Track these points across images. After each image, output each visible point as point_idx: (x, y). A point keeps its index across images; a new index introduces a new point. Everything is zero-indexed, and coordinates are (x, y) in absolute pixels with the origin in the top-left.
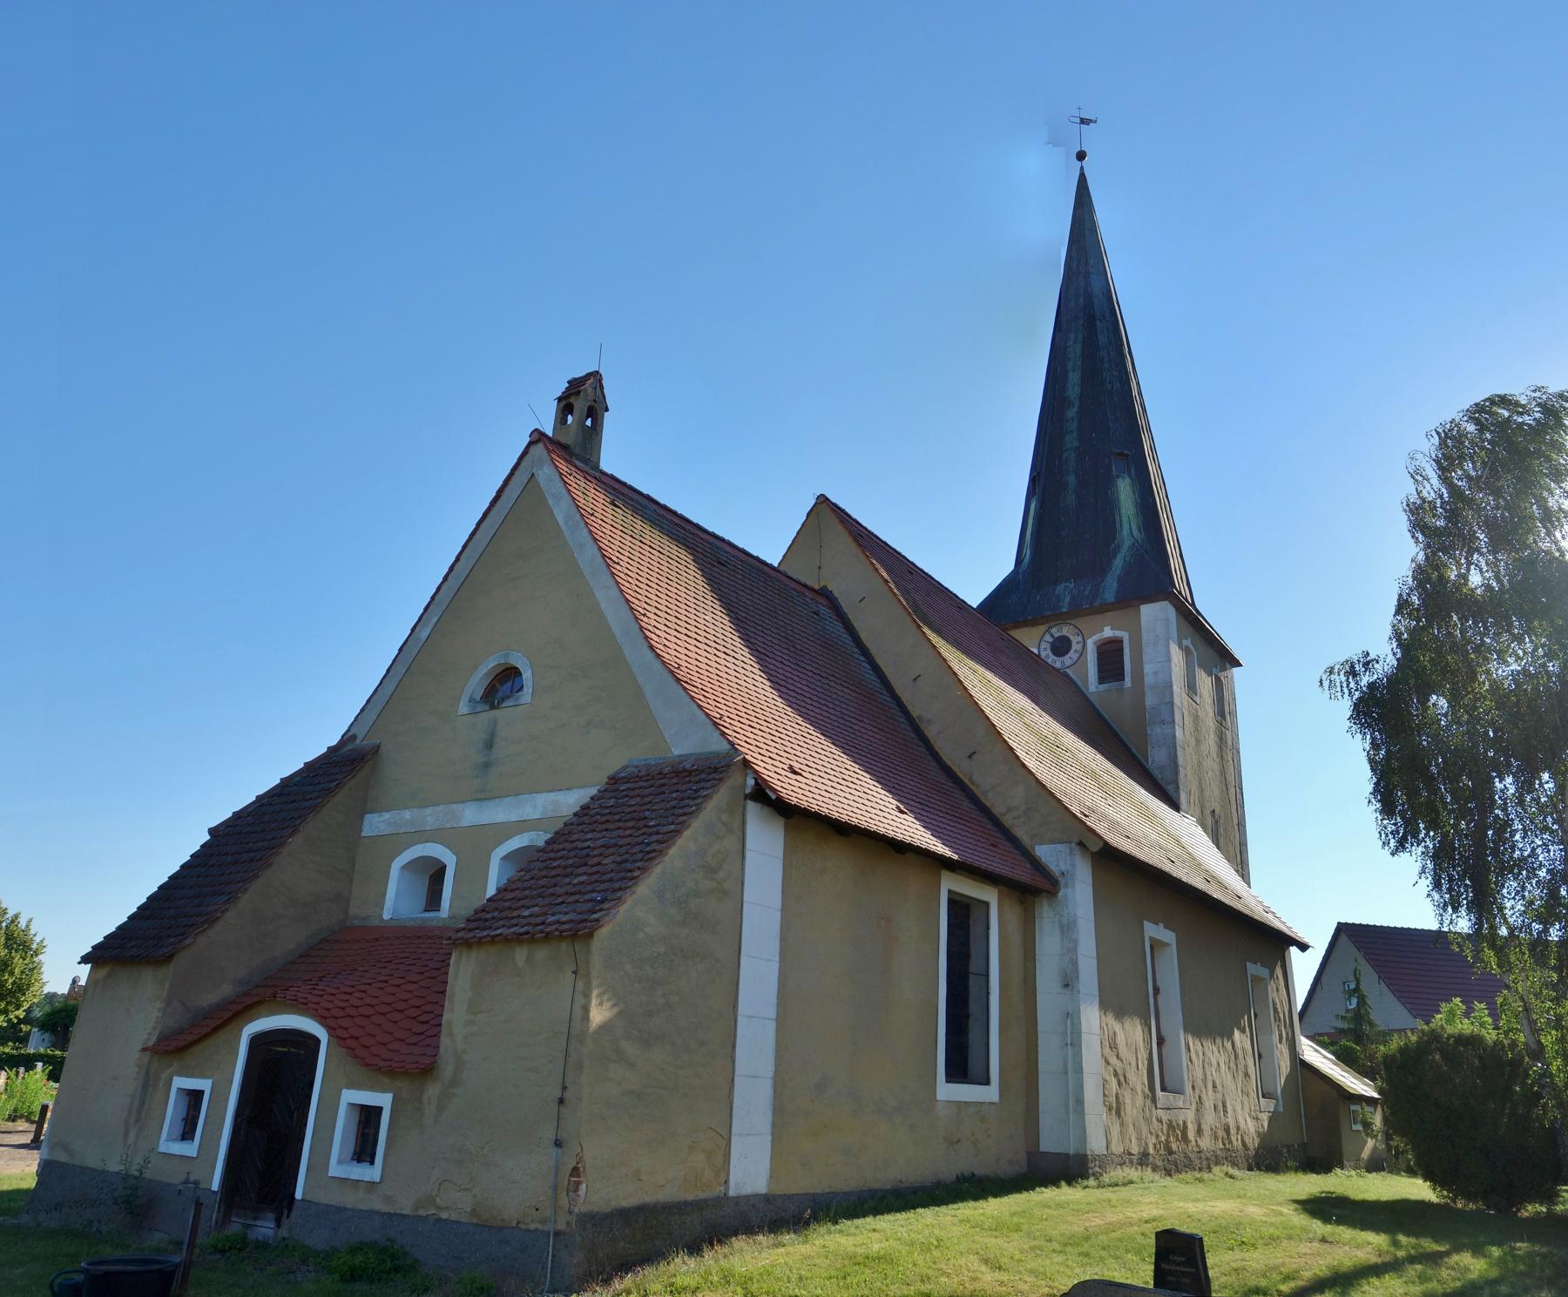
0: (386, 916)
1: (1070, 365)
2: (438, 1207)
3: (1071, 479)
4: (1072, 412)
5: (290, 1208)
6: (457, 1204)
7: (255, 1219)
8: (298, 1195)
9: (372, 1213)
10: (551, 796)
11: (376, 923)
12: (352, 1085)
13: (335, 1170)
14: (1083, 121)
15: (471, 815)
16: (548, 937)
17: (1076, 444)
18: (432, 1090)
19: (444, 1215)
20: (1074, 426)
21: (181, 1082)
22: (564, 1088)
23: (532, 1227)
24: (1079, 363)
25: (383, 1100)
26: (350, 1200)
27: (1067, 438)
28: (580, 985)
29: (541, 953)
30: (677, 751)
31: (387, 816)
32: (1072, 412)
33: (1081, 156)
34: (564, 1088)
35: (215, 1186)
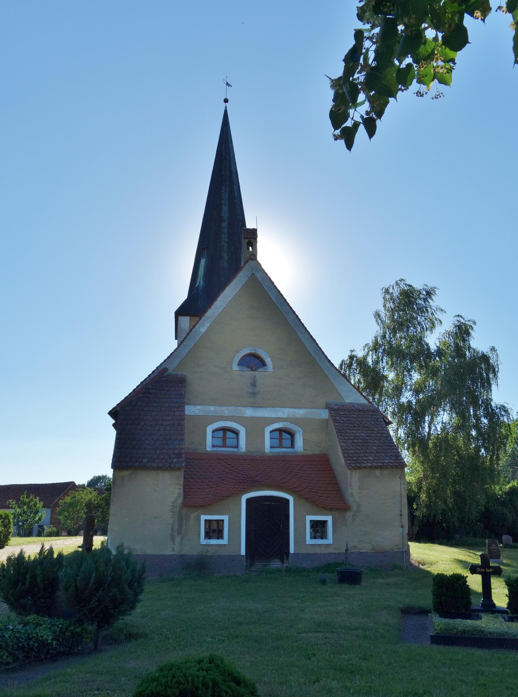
0: (209, 448)
1: (223, 202)
2: (358, 549)
3: (225, 256)
4: (225, 224)
5: (288, 557)
6: (366, 547)
7: (270, 562)
8: (292, 550)
9: (330, 554)
10: (291, 410)
11: (204, 452)
12: (310, 514)
13: (309, 541)
14: (228, 84)
15: (249, 412)
16: (387, 468)
17: (227, 240)
18: (349, 515)
19: (362, 551)
20: (226, 231)
21: (203, 518)
22: (401, 511)
23: (395, 551)
24: (227, 202)
25: (329, 519)
26: (318, 551)
27: (223, 235)
28: (402, 482)
29: (385, 472)
30: (347, 401)
31: (199, 407)
32: (225, 224)
33: (226, 101)
34: (401, 511)
35: (243, 552)
